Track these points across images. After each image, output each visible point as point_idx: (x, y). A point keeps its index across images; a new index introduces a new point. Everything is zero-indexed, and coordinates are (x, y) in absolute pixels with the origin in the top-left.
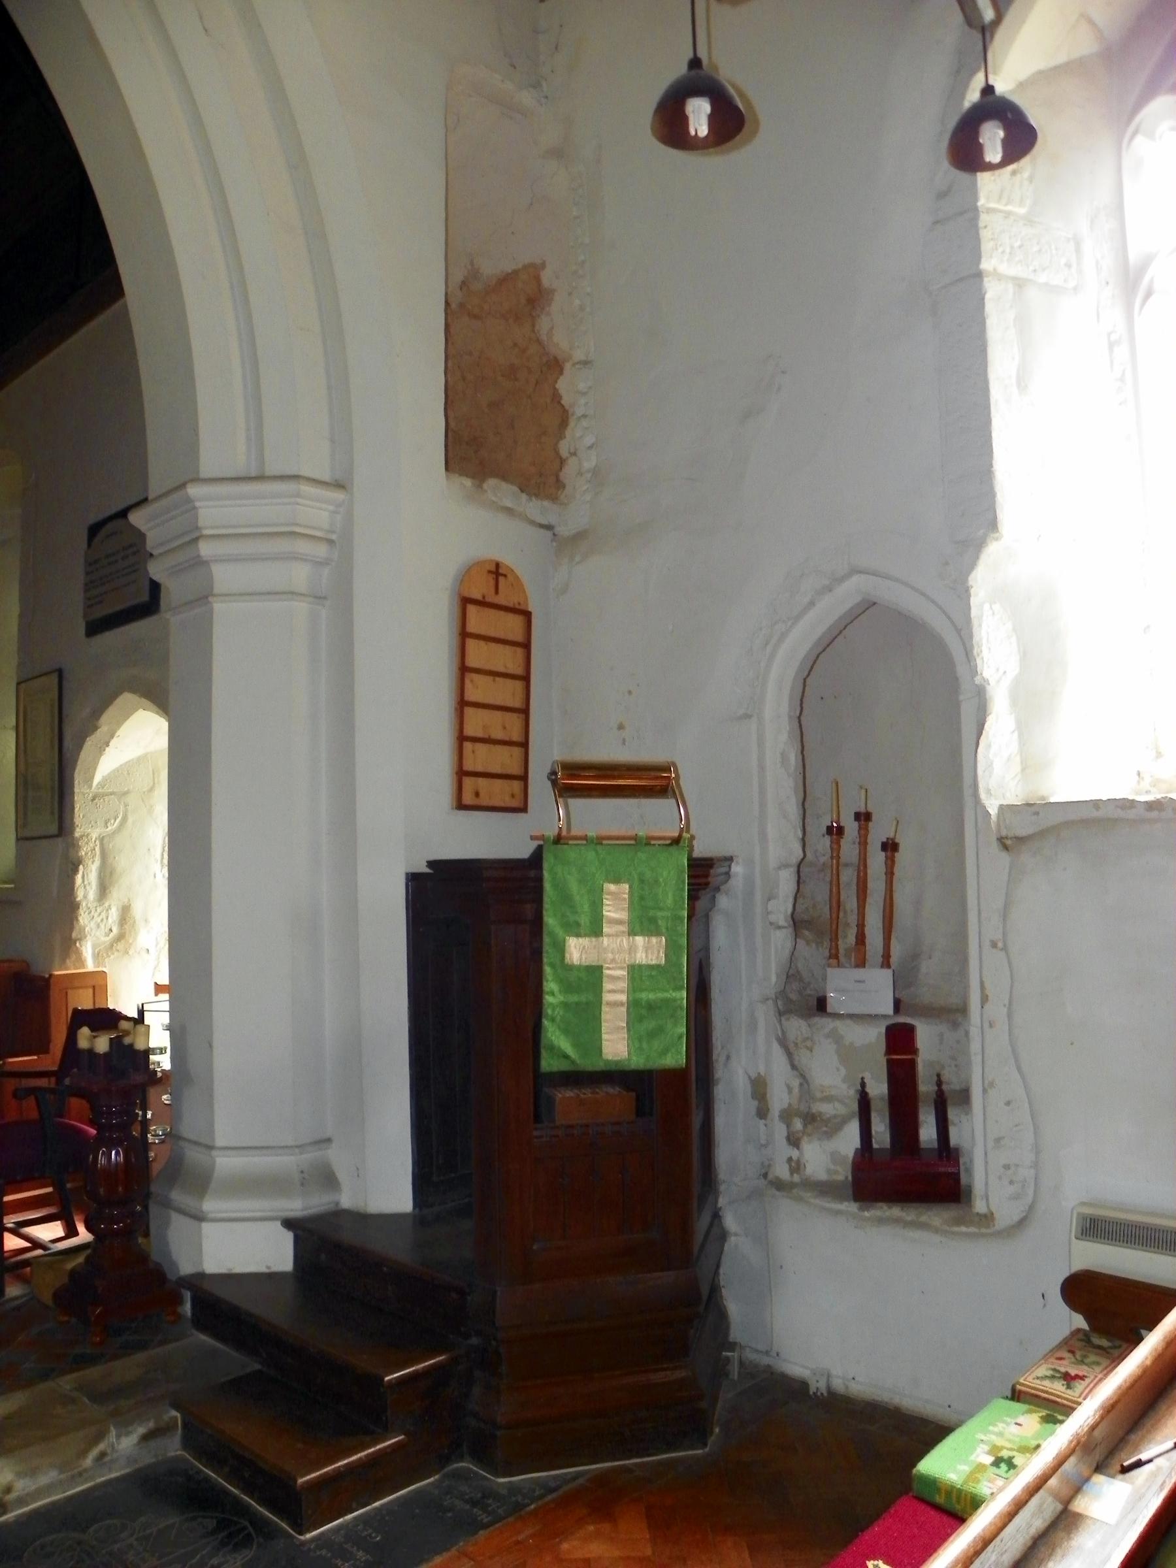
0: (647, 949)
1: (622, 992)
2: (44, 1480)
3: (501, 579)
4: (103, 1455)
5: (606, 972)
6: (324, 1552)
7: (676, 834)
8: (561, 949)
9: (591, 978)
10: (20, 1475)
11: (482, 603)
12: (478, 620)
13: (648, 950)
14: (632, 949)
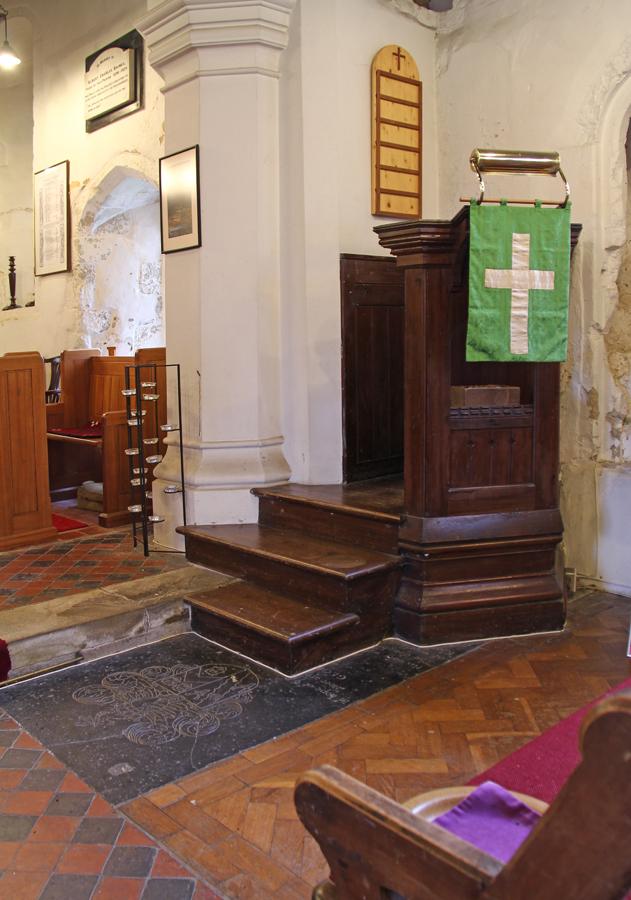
0: (543, 279)
1: (525, 308)
2: (106, 643)
3: (402, 59)
4: (141, 630)
5: (513, 294)
6: (308, 685)
7: (563, 200)
8: (482, 277)
9: (503, 297)
10: (90, 638)
11: (389, 76)
12: (389, 87)
13: (543, 280)
14: (532, 279)
